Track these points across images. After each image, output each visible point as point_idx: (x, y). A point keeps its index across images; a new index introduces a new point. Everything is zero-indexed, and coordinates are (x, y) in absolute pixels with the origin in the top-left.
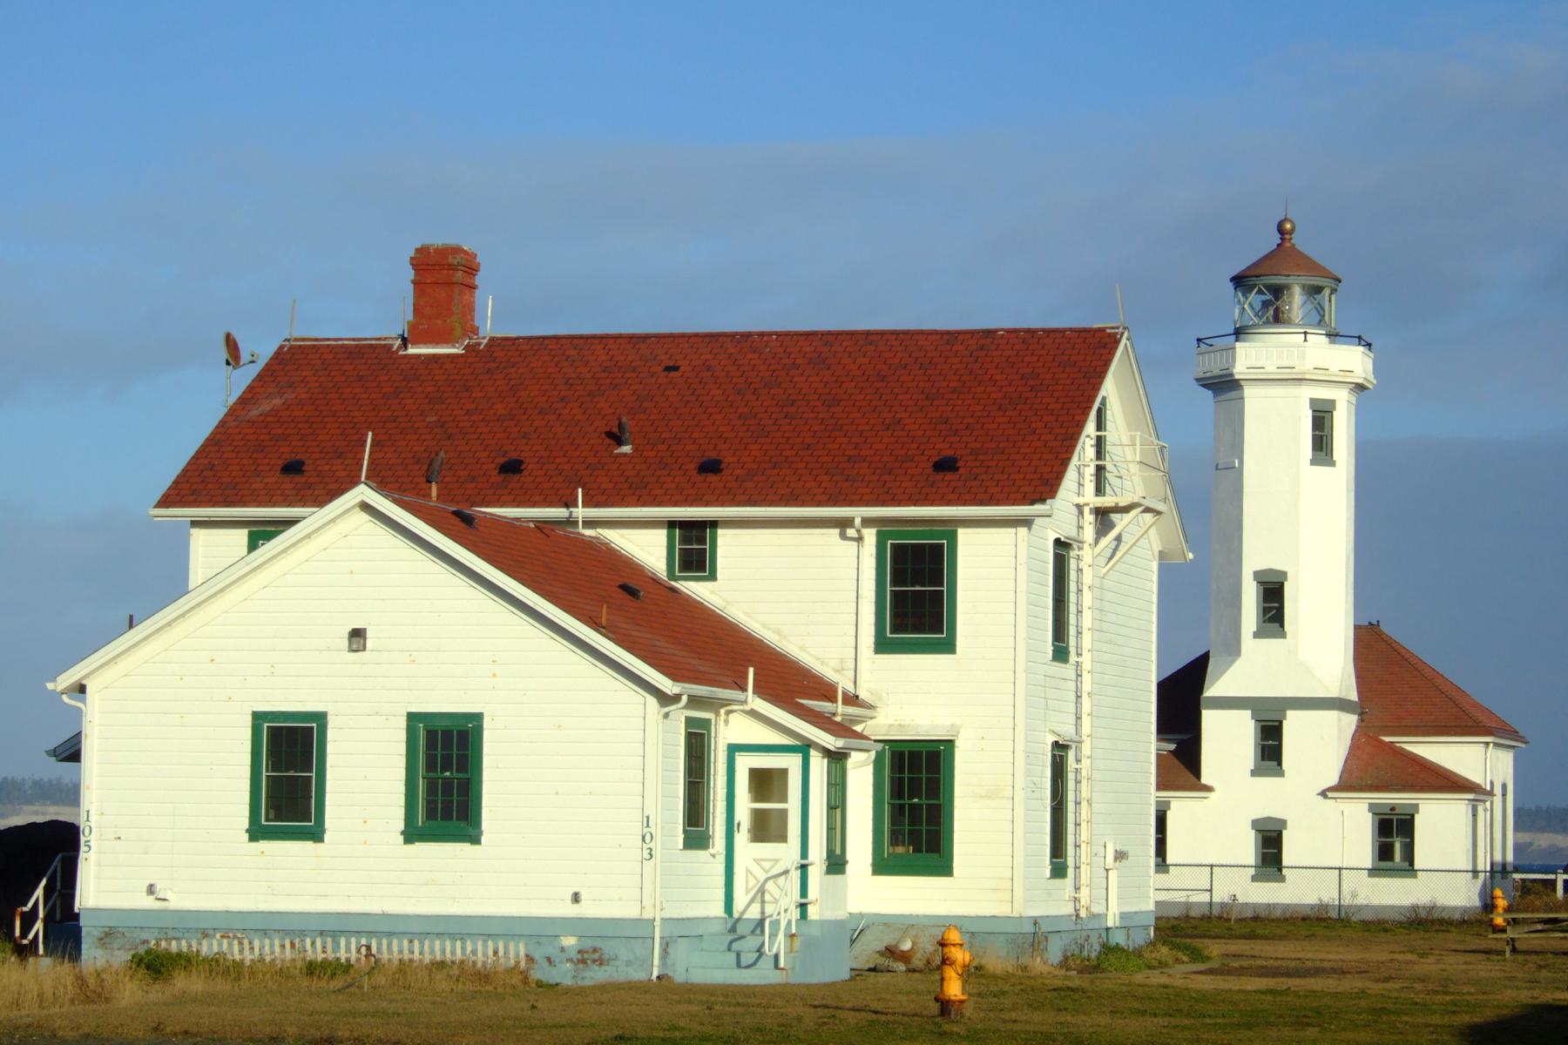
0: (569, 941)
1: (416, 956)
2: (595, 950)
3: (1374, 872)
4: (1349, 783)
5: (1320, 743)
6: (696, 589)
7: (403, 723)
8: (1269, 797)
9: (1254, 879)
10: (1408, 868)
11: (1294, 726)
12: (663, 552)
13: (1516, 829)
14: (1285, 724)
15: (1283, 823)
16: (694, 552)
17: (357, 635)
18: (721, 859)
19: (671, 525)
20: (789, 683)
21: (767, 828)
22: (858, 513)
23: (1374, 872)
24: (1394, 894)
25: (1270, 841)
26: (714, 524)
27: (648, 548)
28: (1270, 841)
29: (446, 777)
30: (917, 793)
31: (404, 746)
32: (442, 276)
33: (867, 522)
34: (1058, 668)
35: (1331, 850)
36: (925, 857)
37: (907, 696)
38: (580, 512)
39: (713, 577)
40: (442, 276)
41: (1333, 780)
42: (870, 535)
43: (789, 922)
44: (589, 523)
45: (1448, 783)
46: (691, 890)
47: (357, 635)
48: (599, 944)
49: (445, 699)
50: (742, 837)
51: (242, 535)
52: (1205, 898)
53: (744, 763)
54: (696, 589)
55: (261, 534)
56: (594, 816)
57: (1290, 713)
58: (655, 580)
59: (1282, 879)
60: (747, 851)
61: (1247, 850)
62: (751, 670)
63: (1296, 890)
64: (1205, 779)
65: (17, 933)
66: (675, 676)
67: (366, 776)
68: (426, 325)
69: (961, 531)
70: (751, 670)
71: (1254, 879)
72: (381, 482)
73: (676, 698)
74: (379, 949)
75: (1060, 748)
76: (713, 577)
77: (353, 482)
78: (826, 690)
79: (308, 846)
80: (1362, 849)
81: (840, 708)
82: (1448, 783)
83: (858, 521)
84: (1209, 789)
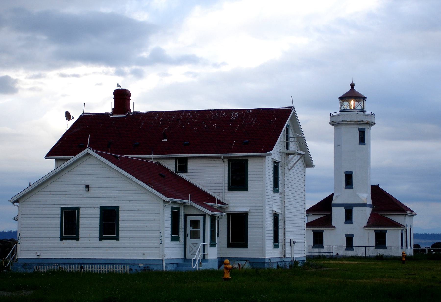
0: (141, 265)
1: (45, 270)
2: (148, 267)
4: (369, 225)
5: (362, 215)
7: (99, 209)
8: (349, 229)
9: (346, 250)
11: (355, 210)
12: (174, 166)
16: (182, 165)
17: (88, 187)
18: (183, 243)
19: (176, 159)
20: (202, 197)
21: (195, 235)
22: (222, 155)
24: (349, 253)
25: (349, 239)
26: (187, 159)
27: (171, 166)
28: (349, 239)
30: (238, 227)
31: (99, 215)
33: (224, 157)
34: (276, 195)
35: (365, 242)
37: (237, 202)
38: (152, 156)
39: (186, 172)
40: (122, 97)
41: (366, 225)
42: (226, 160)
43: (199, 259)
47: (88, 187)
48: (148, 265)
49: (109, 203)
50: (188, 238)
52: (331, 254)
53: (189, 219)
56: (148, 234)
57: (354, 208)
58: (171, 173)
59: (353, 250)
60: (190, 242)
61: (344, 243)
62: (190, 195)
63: (357, 252)
64: (333, 224)
65: (192, 266)
67: (89, 223)
68: (115, 111)
69: (249, 159)
70: (190, 195)
71: (346, 250)
72: (94, 147)
73: (168, 202)
74: (65, 268)
75: (276, 218)
76: (186, 172)
77: (84, 148)
78: (212, 199)
79: (75, 242)
81: (217, 205)
83: (222, 157)
84: (334, 227)
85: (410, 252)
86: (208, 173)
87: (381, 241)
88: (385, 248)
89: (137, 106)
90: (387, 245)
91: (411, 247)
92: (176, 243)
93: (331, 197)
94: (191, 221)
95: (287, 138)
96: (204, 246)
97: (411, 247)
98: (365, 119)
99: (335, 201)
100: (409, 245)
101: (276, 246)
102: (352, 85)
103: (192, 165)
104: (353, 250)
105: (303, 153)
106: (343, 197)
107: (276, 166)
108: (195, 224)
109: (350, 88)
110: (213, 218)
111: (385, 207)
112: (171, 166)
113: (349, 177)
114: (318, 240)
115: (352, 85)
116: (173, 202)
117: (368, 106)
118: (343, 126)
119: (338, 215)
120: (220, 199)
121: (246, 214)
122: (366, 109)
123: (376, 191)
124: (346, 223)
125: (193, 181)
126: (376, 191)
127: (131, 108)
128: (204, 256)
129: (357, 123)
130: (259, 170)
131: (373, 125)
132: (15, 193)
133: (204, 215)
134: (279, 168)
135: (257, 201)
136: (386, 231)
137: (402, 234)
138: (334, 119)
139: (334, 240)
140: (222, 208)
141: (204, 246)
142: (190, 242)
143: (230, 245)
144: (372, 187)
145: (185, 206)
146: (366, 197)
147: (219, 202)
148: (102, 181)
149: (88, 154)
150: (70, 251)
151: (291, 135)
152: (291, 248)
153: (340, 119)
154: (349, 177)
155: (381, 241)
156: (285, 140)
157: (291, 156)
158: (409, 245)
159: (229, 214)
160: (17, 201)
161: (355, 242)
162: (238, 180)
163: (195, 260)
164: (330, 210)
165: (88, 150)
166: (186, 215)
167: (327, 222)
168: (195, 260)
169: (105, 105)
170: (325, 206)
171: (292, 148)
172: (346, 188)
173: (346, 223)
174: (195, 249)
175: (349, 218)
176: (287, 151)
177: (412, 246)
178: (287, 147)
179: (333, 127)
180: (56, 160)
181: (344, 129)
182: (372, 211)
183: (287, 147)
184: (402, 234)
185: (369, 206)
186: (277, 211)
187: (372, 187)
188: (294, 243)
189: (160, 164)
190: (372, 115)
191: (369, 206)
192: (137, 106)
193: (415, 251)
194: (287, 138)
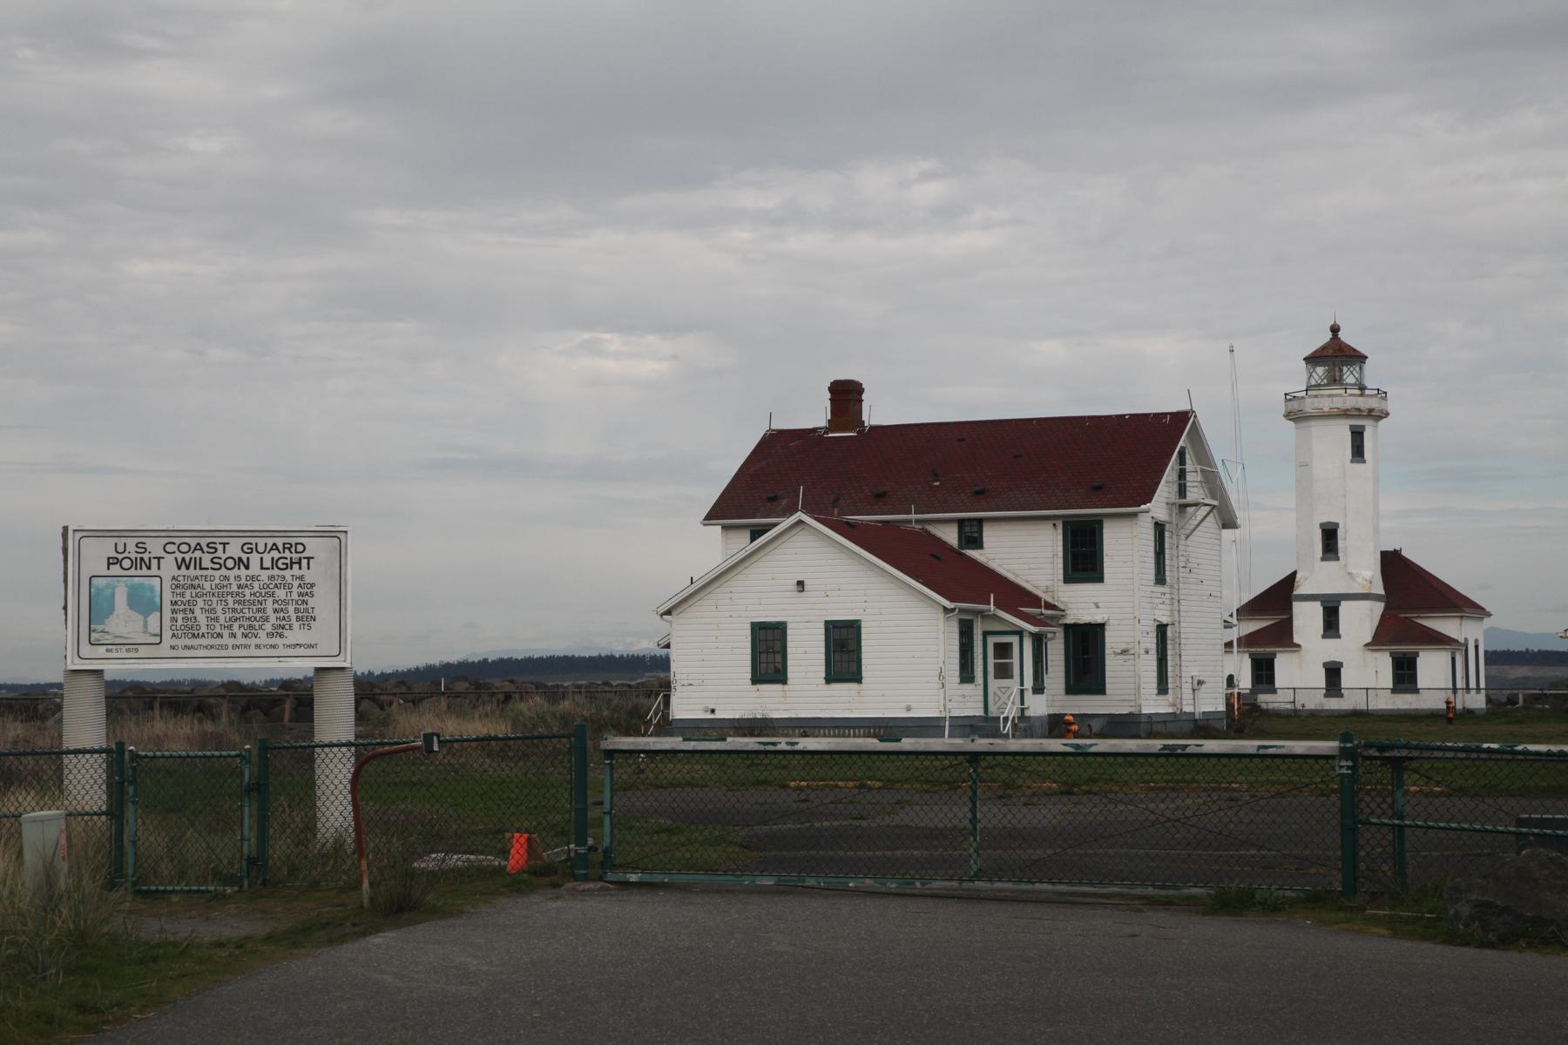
3: (1394, 690)
4: (1381, 638)
5: (1360, 620)
6: (973, 553)
7: (822, 625)
8: (1331, 650)
10: (1098, 688)
11: (1345, 609)
13: (1487, 663)
14: (1341, 609)
15: (1341, 664)
17: (800, 583)
19: (961, 522)
20: (1015, 597)
21: (1003, 672)
23: (1394, 690)
24: (1405, 702)
25: (1333, 672)
26: (980, 521)
27: (950, 535)
28: (1333, 672)
29: (844, 650)
30: (1086, 645)
32: (846, 395)
34: (1160, 589)
35: (1369, 679)
36: (1265, 686)
37: (1081, 603)
38: (913, 516)
39: (981, 547)
40: (846, 395)
44: (917, 521)
45: (1439, 640)
46: (967, 702)
47: (800, 583)
51: (747, 535)
52: (1289, 706)
53: (991, 640)
54: (973, 553)
55: (756, 533)
56: (914, 666)
58: (951, 548)
59: (1341, 696)
60: (994, 684)
61: (1320, 680)
64: (1296, 640)
66: (951, 600)
67: (806, 652)
68: (834, 424)
73: (953, 610)
75: (1162, 630)
76: (981, 547)
78: (1035, 600)
80: (1387, 679)
82: (1439, 640)
84: (1299, 646)
85: (1477, 701)
86: (1024, 551)
87: (1405, 674)
88: (1416, 691)
89: (878, 411)
90: (1421, 684)
91: (1478, 689)
92: (968, 687)
93: (1291, 580)
94: (996, 645)
95: (1182, 475)
96: (1022, 691)
97: (1478, 689)
98: (1363, 403)
99: (1301, 589)
100: (1473, 684)
101: (1163, 688)
102: (1335, 330)
103: (990, 535)
104: (1341, 696)
105: (1216, 503)
106: (1318, 578)
107: (1159, 528)
108: (1003, 650)
109: (1330, 335)
110: (1039, 641)
111: (1413, 599)
112: (950, 535)
113: (1330, 536)
114: (1264, 672)
115: (1335, 330)
116: (962, 611)
117: (1373, 374)
118: (1313, 423)
119: (1307, 618)
120: (1050, 600)
121: (1102, 626)
122: (1368, 384)
123: (1394, 565)
124: (1324, 637)
125: (993, 565)
126: (1394, 565)
127: (865, 417)
128: (1023, 710)
129: (1345, 414)
130: (1126, 545)
131: (1381, 418)
132: (667, 596)
133: (1020, 633)
134: (1167, 534)
135: (1120, 600)
136: (1417, 654)
137: (1453, 659)
138: (1295, 406)
139: (1298, 677)
140: (1052, 617)
141: (1022, 691)
142: (994, 684)
143: (1071, 690)
144: (1384, 555)
145: (984, 615)
146: (1368, 575)
147: (1049, 606)
148: (817, 572)
149: (800, 522)
150: (772, 702)
151: (1189, 466)
152: (422, 700)
153: (1309, 406)
154: (1330, 536)
155: (1405, 674)
156: (1175, 478)
157: (1190, 510)
158: (1473, 684)
159: (1067, 627)
160: (668, 612)
161: (1346, 680)
162: (1084, 561)
163: (1006, 719)
164: (1290, 608)
165: (799, 515)
166: (986, 634)
167: (1282, 635)
168: (1006, 719)
169: (815, 414)
170: (1277, 601)
171: (1194, 494)
172: (1323, 559)
173: (1324, 637)
174: (1004, 698)
175: (1331, 626)
176: (1183, 501)
177: (1482, 685)
178: (1182, 491)
179: (1291, 424)
180: (725, 528)
181: (1317, 429)
182: (1386, 609)
183: (1182, 491)
184: (1453, 659)
185: (1376, 597)
186: (1165, 620)
187: (1384, 555)
188: (1200, 683)
189: (928, 533)
190: (1382, 395)
191: (1376, 597)
192: (878, 411)
193: (1489, 700)
194: (1182, 475)
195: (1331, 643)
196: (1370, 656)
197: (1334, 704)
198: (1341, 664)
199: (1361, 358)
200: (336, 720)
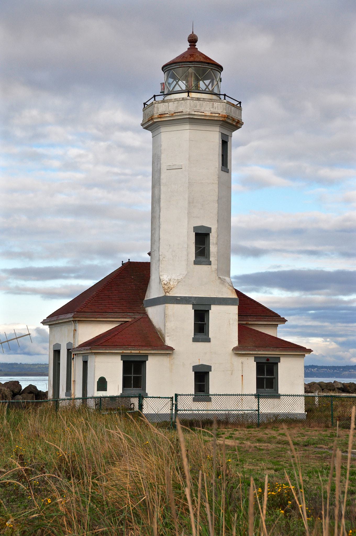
8: (199, 354)
10: (105, 389)
15: (209, 368)
25: (202, 376)
28: (202, 376)
59: (209, 400)
64: (169, 342)
80: (251, 387)
84: (171, 349)
87: (267, 379)
90: (280, 391)
102: (193, 41)
115: (193, 41)
136: (146, 356)
155: (267, 379)
161: (214, 386)
182: (214, 304)
195: (201, 345)
196: (238, 361)
197: (268, 407)
198: (209, 368)
199: (220, 68)
200: (311, 380)
